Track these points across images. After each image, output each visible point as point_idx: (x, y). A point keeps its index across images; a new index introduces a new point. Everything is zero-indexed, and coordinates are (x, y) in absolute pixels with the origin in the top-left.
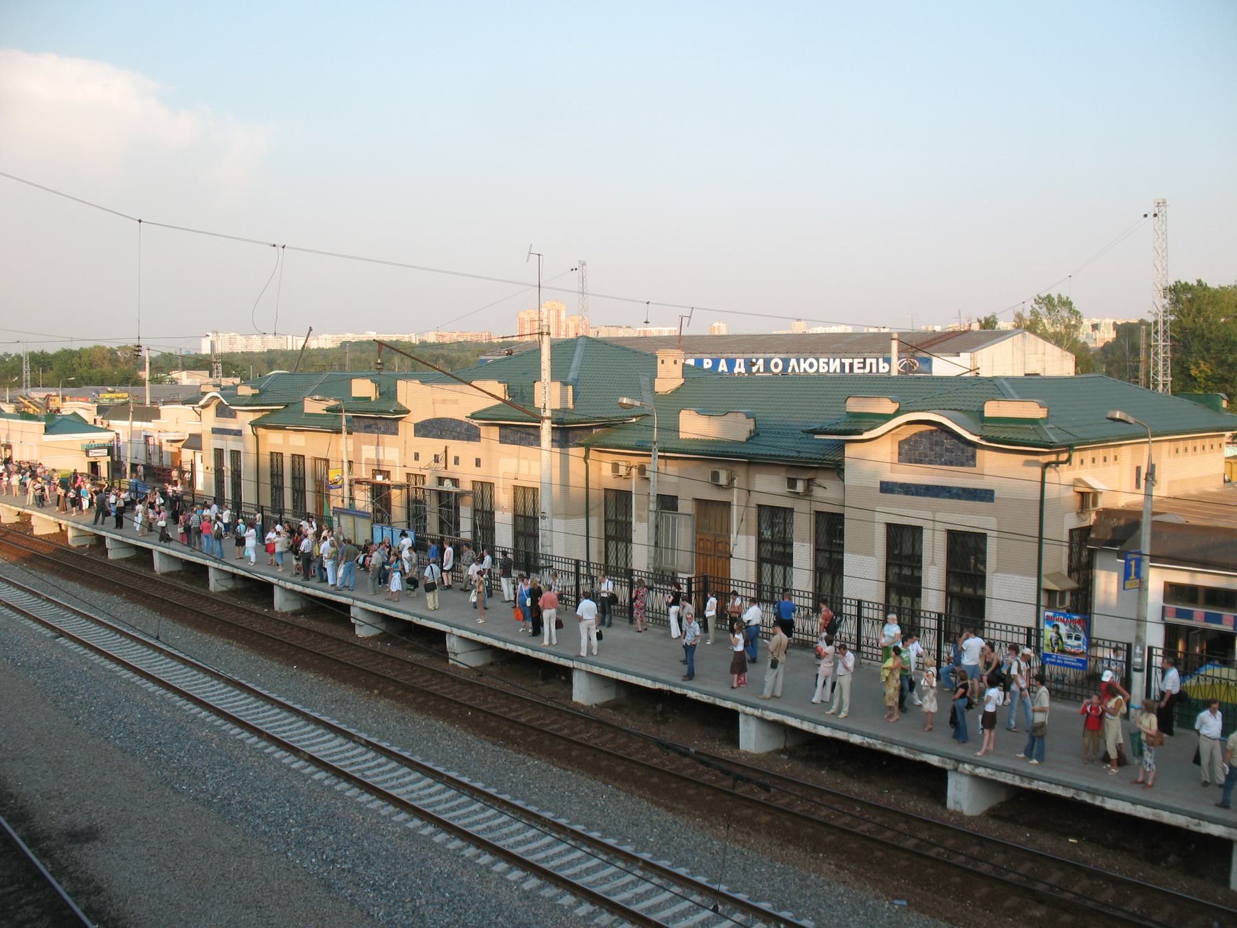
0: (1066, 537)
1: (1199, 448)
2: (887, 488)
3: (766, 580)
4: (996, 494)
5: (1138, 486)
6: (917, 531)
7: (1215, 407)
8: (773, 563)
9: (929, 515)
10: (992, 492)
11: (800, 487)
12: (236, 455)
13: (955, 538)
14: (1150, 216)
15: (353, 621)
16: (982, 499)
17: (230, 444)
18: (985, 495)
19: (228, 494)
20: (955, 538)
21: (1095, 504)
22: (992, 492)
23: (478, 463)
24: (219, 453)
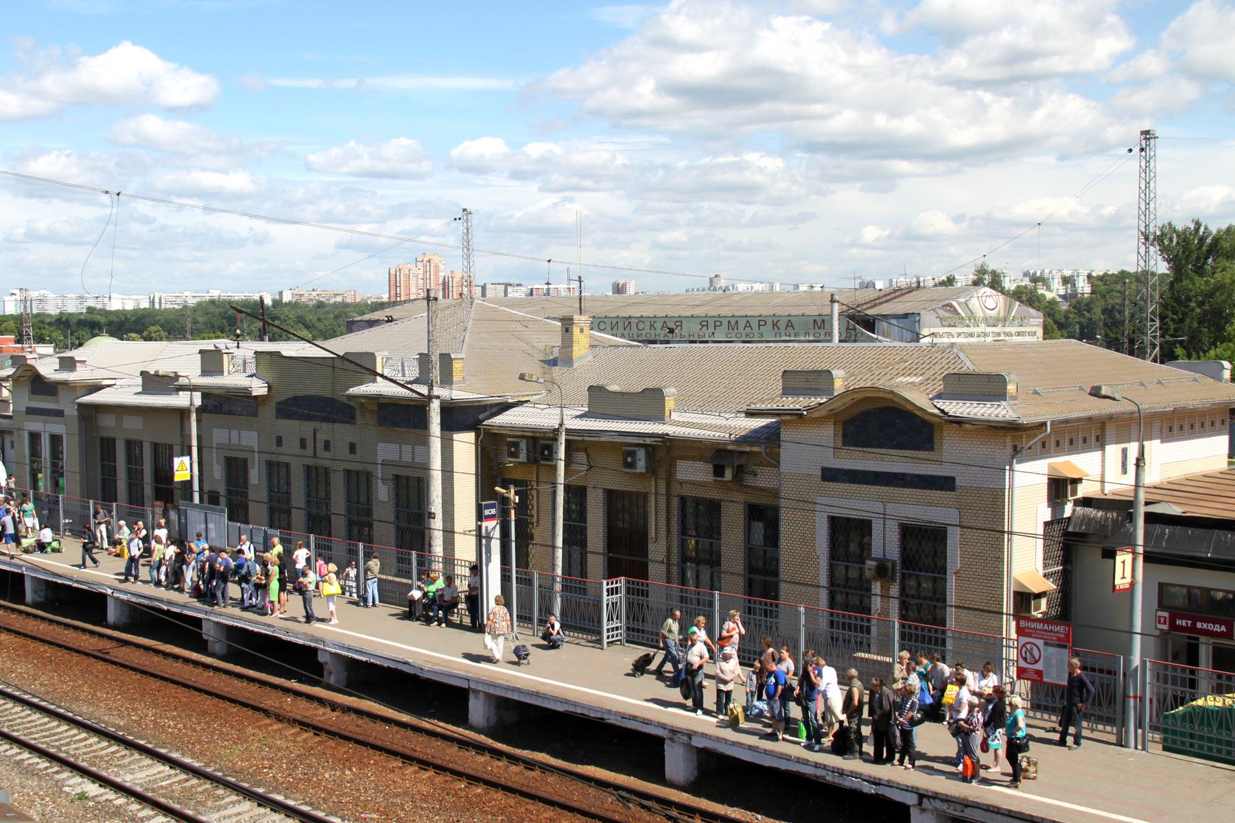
0: (1040, 531)
1: (1197, 426)
2: (830, 475)
3: (322, 486)
4: (958, 483)
5: (1125, 471)
6: (864, 527)
7: (1218, 378)
8: (697, 561)
9: (878, 507)
10: (952, 479)
11: (728, 475)
12: (56, 440)
13: (909, 532)
14: (1136, 150)
15: (205, 637)
16: (942, 488)
17: (47, 428)
18: (946, 484)
19: (484, 541)
20: (909, 532)
21: (1074, 492)
22: (952, 479)
23: (352, 448)
24: (35, 437)
